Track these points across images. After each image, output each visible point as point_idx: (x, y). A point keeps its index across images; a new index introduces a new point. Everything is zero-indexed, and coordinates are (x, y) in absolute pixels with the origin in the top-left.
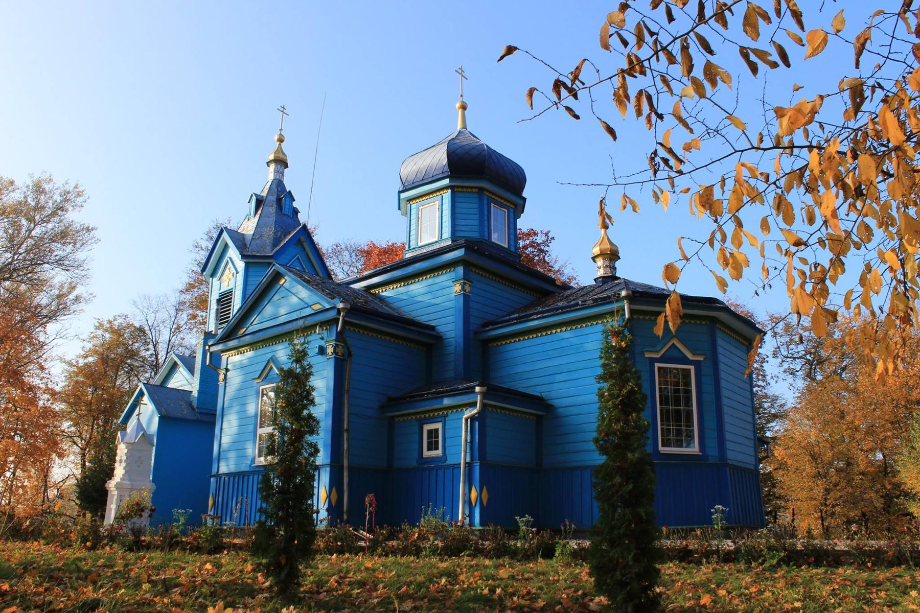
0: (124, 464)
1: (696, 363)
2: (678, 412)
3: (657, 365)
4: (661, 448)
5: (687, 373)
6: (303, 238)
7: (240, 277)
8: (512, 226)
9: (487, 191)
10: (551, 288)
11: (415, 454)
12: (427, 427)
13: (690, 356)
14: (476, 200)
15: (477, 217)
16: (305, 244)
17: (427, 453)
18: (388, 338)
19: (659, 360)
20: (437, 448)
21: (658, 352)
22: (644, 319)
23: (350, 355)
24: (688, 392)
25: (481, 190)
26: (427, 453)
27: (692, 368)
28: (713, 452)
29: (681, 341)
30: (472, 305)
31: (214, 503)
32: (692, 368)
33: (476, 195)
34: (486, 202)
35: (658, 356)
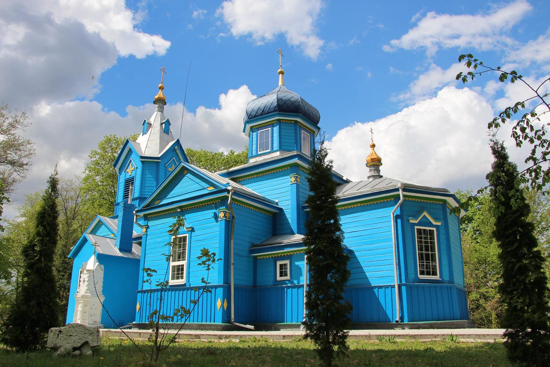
0: (86, 283)
1: (437, 227)
2: (427, 255)
3: (416, 227)
4: (419, 276)
5: (431, 232)
6: (176, 147)
7: (139, 171)
8: (313, 143)
9: (300, 123)
10: (341, 182)
11: (272, 279)
12: (279, 263)
13: (434, 223)
14: (293, 128)
15: (293, 138)
16: (178, 151)
17: (279, 278)
18: (253, 208)
19: (419, 224)
20: (182, 278)
21: (417, 219)
22: (387, 201)
23: (233, 217)
24: (432, 243)
25: (296, 122)
26: (279, 278)
27: (434, 229)
28: (446, 278)
29: (430, 213)
30: (301, 190)
31: (140, 308)
32: (434, 229)
33: (293, 125)
34: (299, 129)
35: (416, 222)
